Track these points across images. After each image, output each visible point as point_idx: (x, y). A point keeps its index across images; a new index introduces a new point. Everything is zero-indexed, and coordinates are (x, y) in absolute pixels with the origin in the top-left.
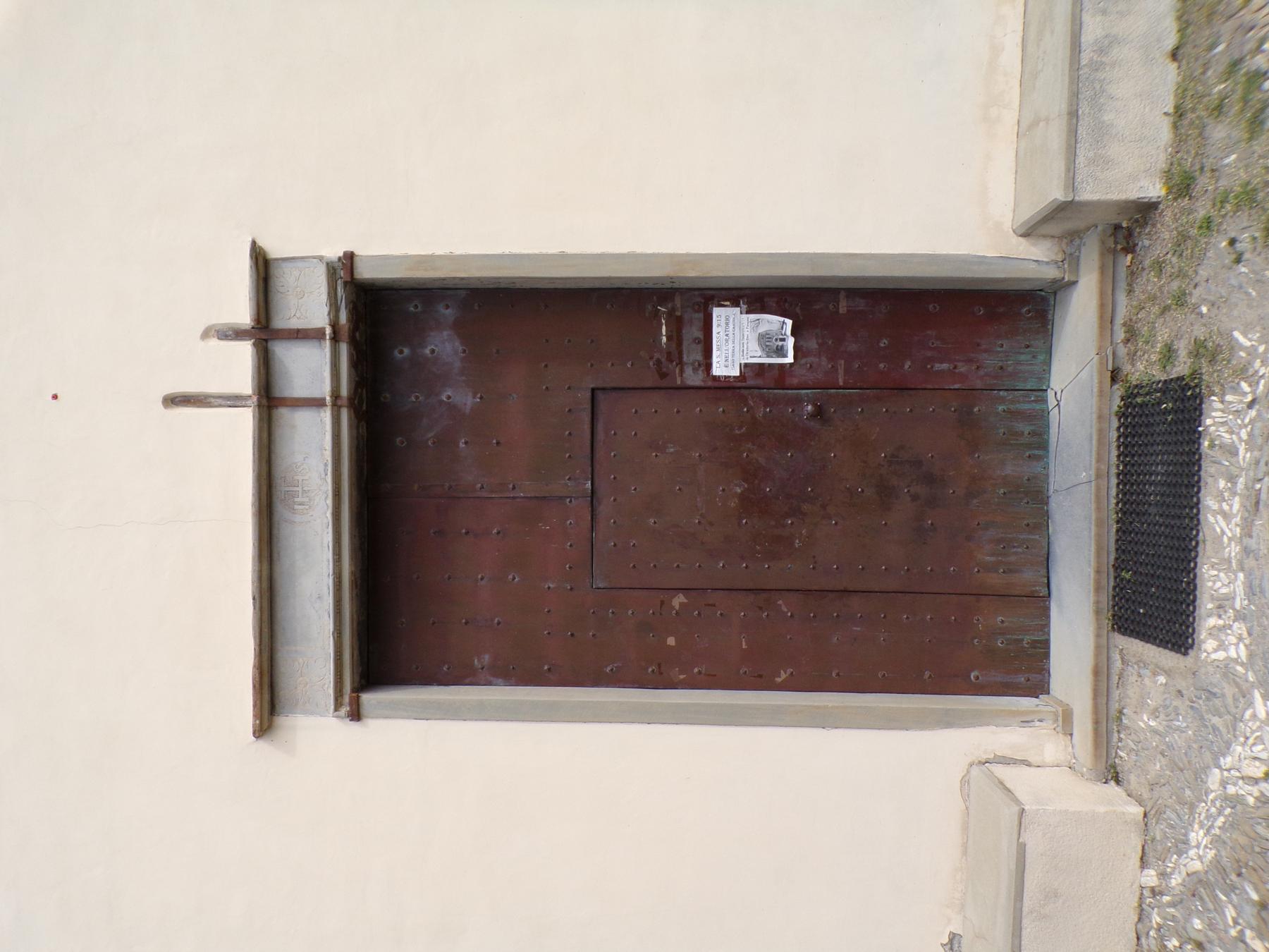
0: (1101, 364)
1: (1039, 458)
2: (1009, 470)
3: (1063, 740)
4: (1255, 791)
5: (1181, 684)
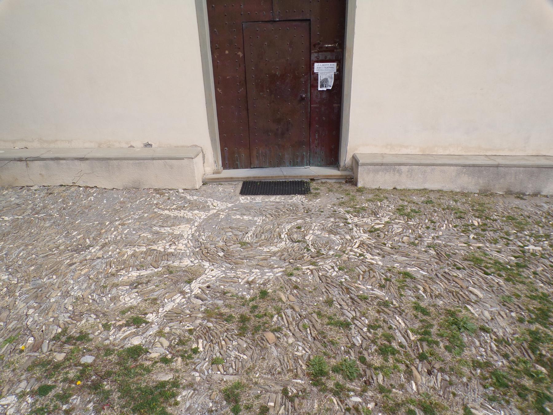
1: (290, 164)
2: (286, 156)
3: (212, 172)
5: (232, 194)
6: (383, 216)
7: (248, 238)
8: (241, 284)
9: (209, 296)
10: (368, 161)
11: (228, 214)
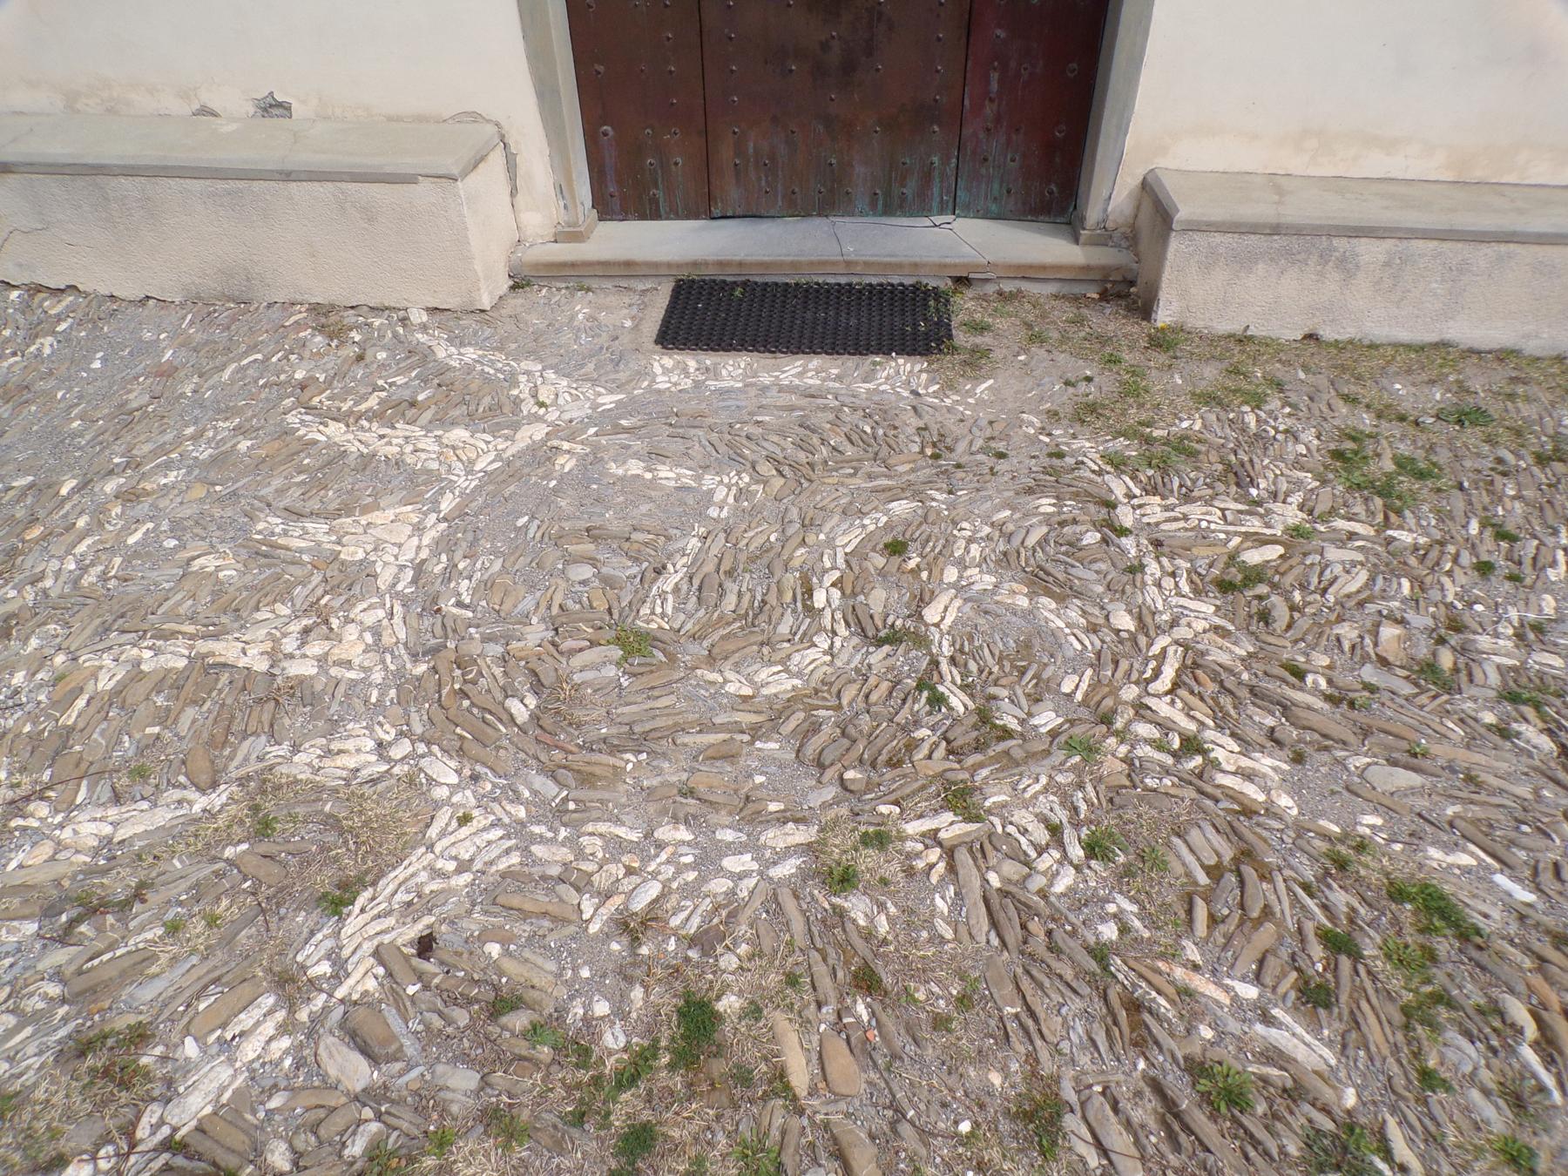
0: (978, 266)
2: (860, 170)
3: (549, 232)
4: (525, 395)
5: (625, 339)
6: (1274, 496)
7: (660, 611)
8: (594, 928)
9: (414, 1025)
10: (1217, 214)
11: (596, 448)
